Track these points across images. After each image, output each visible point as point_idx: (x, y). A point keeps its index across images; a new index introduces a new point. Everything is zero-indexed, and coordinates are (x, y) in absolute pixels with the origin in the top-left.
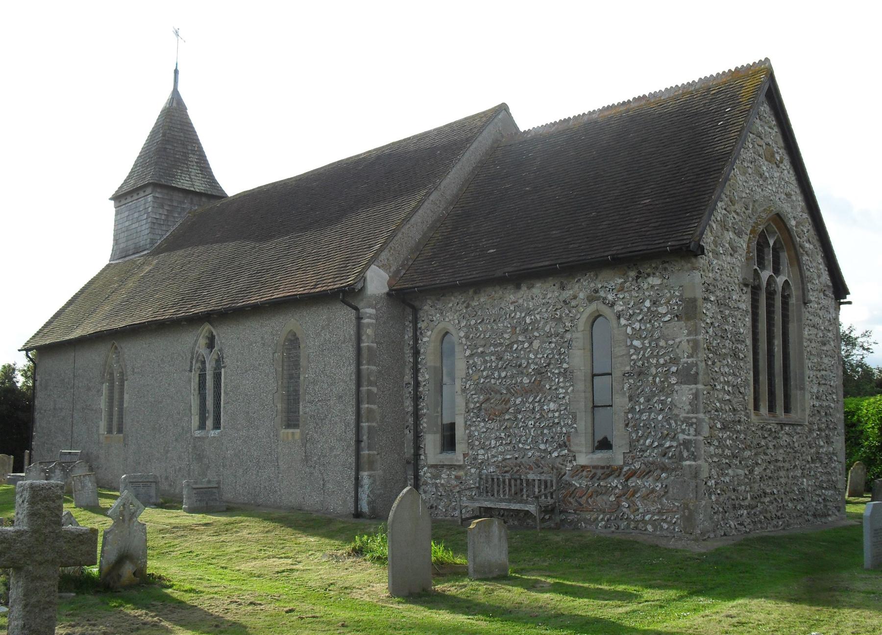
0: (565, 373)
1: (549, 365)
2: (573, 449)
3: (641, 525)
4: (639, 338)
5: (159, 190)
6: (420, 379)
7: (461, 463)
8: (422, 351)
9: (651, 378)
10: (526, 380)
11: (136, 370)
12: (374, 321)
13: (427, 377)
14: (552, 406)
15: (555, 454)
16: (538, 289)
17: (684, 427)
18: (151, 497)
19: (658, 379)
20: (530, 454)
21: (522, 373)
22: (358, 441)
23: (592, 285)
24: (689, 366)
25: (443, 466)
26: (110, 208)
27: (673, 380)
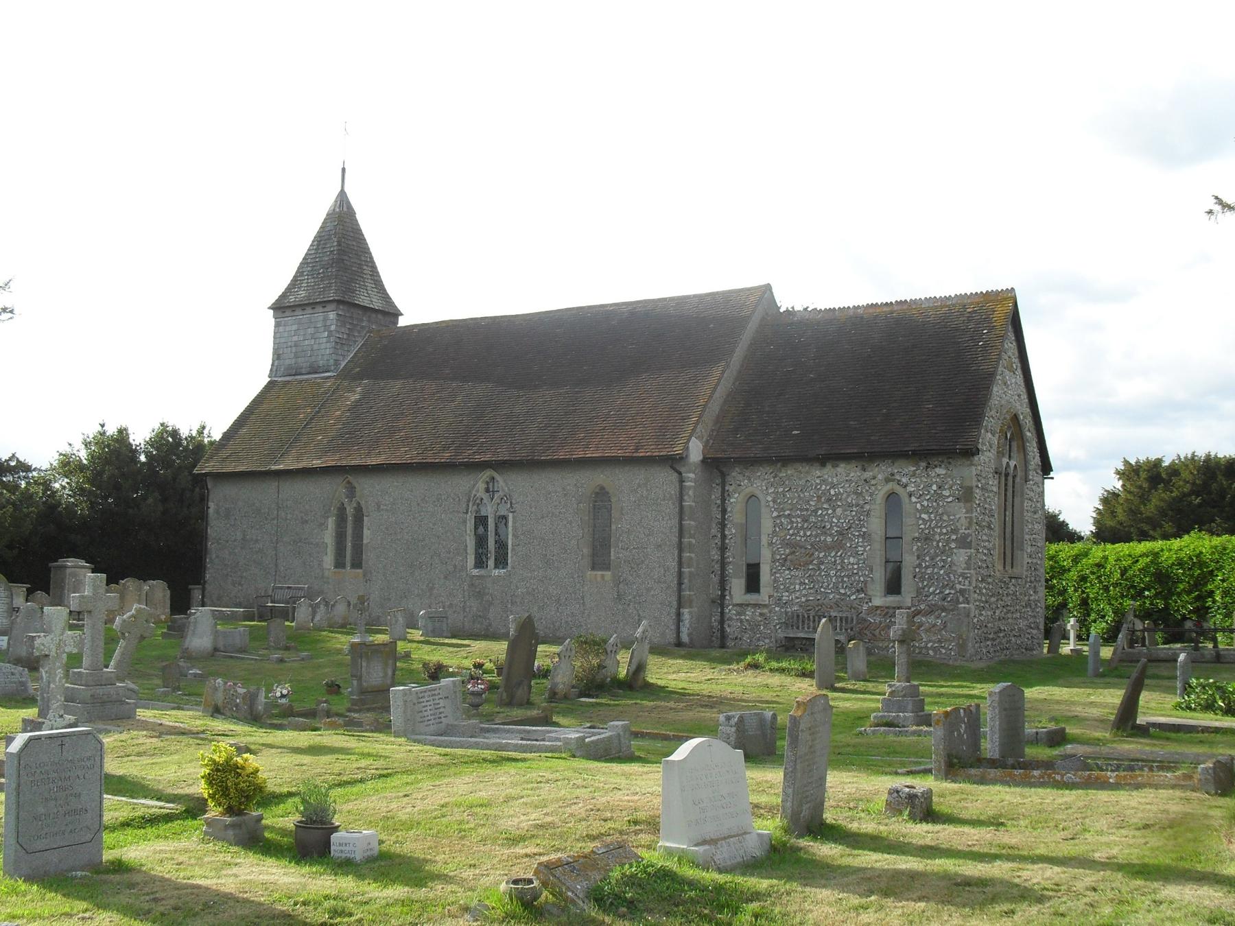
0: (864, 536)
1: (850, 528)
2: (870, 593)
3: (924, 651)
4: (927, 513)
5: (341, 307)
6: (726, 533)
7: (767, 603)
8: (729, 509)
9: (935, 543)
10: (829, 539)
11: (382, 507)
12: (693, 484)
13: (734, 531)
14: (852, 560)
15: (853, 597)
16: (842, 468)
17: (960, 579)
18: (443, 631)
19: (940, 544)
20: (831, 596)
21: (826, 533)
22: (680, 584)
23: (889, 469)
24: (965, 536)
25: (748, 605)
26: (269, 319)
27: (953, 545)
